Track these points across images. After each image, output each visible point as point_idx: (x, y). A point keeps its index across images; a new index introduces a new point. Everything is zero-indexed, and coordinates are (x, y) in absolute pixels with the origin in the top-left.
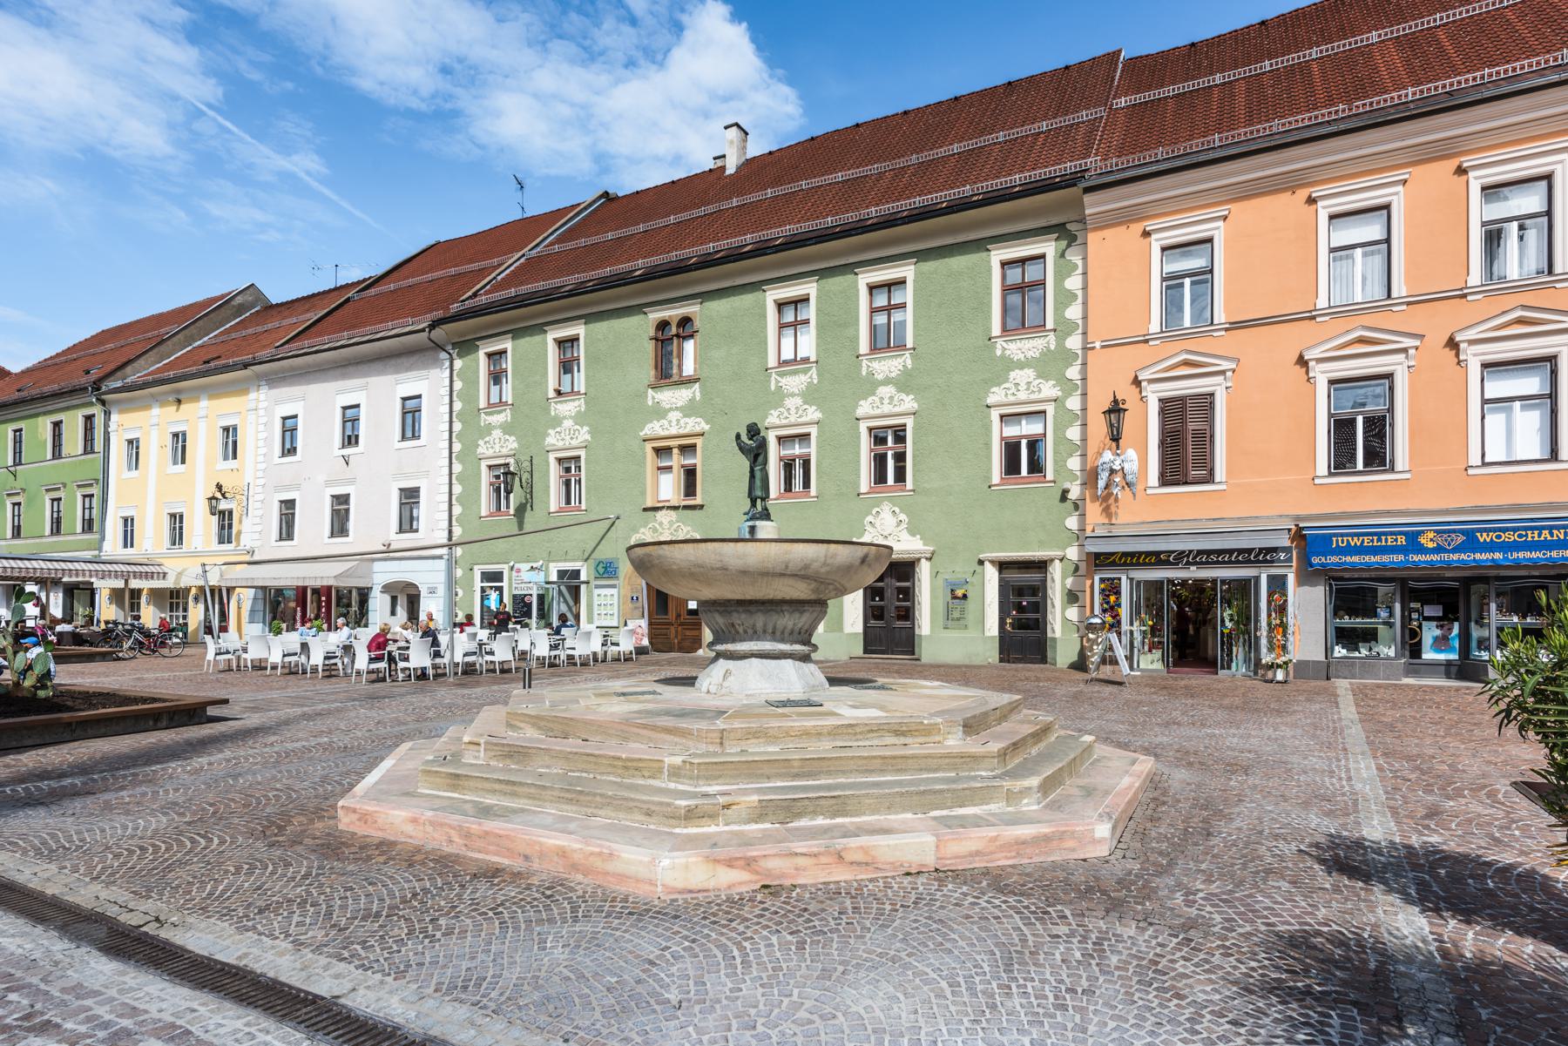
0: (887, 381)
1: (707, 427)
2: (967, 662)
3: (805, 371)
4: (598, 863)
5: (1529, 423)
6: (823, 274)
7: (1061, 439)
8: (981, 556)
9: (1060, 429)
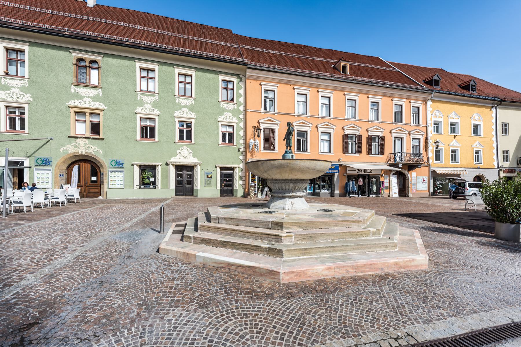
0: (185, 107)
1: (105, 108)
2: (212, 197)
3: (154, 96)
4: (409, 264)
5: (326, 144)
6: (161, 63)
7: (238, 134)
8: (133, 163)
9: (238, 131)
